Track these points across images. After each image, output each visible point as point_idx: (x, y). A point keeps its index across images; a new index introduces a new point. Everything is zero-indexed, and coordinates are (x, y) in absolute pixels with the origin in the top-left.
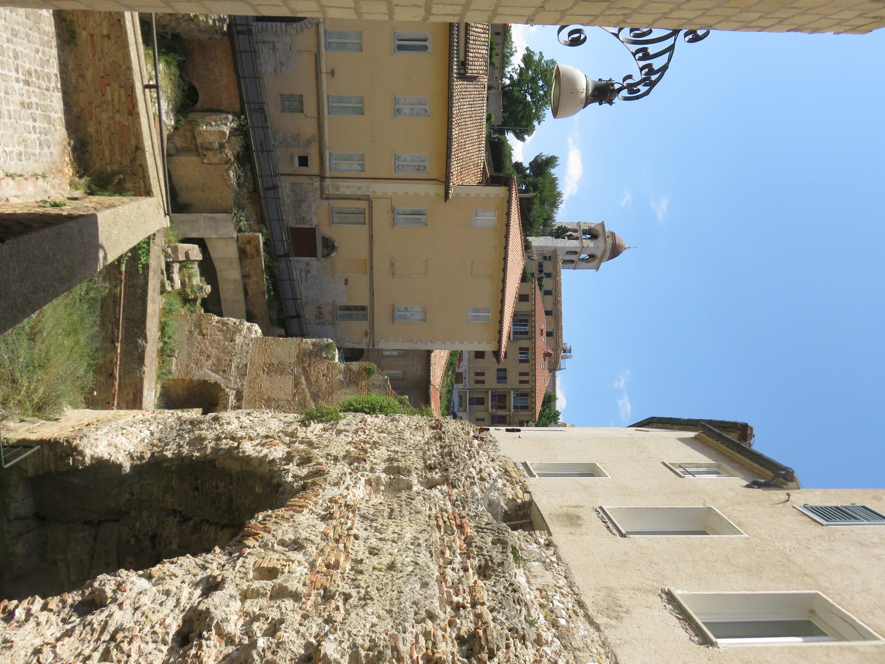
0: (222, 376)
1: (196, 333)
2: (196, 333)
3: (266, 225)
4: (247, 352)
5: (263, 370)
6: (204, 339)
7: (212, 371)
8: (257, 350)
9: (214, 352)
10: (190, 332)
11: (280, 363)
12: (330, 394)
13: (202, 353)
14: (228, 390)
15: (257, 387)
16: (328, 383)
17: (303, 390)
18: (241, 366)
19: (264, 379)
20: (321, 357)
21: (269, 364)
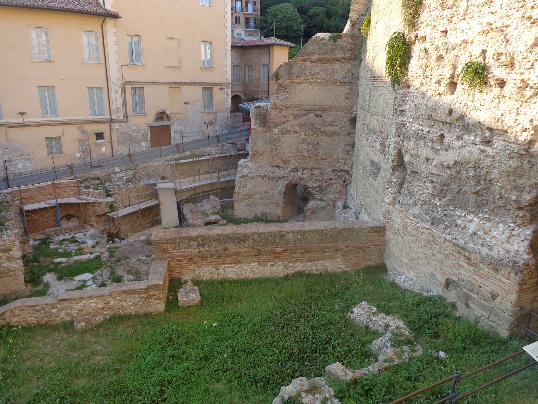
15: (288, 159)
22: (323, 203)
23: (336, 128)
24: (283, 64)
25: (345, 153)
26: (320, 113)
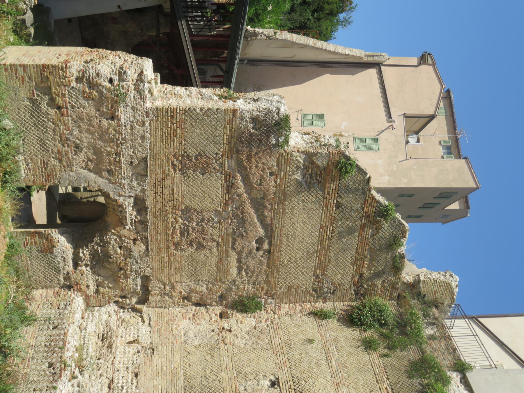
0: (108, 179)
1: (44, 106)
2: (44, 106)
3: (142, 317)
4: (143, 138)
5: (174, 166)
6: (62, 115)
7: (90, 170)
8: (159, 133)
9: (86, 139)
10: (33, 101)
11: (200, 155)
12: (281, 202)
13: (64, 140)
14: (121, 199)
15: (166, 192)
16: (277, 186)
17: (240, 196)
18: (136, 162)
19: (177, 180)
20: (269, 146)
21: (183, 156)
22: (71, 263)
23: (235, 275)
24: (368, 176)
25: (183, 293)
26: (266, 246)
